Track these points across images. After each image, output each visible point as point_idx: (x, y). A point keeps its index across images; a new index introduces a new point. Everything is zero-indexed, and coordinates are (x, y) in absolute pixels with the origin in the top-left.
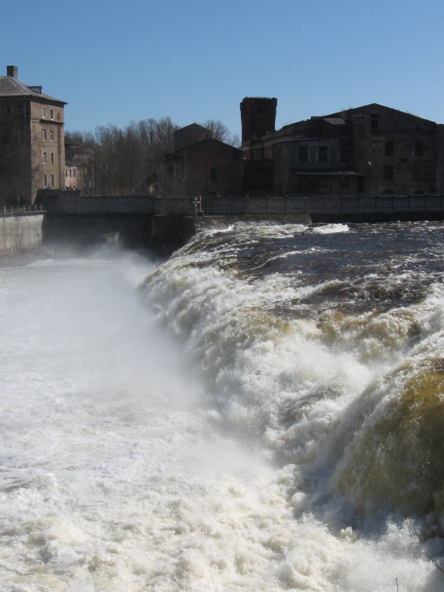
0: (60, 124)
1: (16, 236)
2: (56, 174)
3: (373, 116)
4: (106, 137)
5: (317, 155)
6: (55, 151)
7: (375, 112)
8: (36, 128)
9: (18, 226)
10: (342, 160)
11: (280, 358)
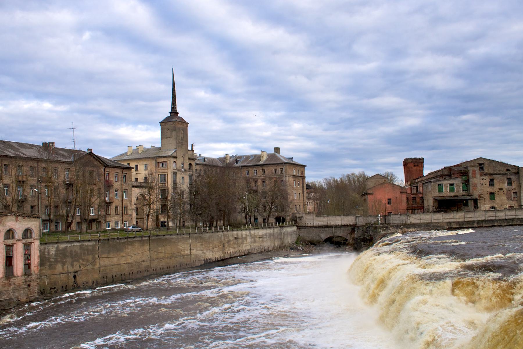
0: (303, 178)
1: (281, 239)
2: (302, 204)
3: (480, 164)
4: (329, 184)
5: (448, 188)
6: (301, 192)
7: (481, 162)
8: (289, 180)
9: (281, 233)
10: (463, 191)
11: (100, 223)
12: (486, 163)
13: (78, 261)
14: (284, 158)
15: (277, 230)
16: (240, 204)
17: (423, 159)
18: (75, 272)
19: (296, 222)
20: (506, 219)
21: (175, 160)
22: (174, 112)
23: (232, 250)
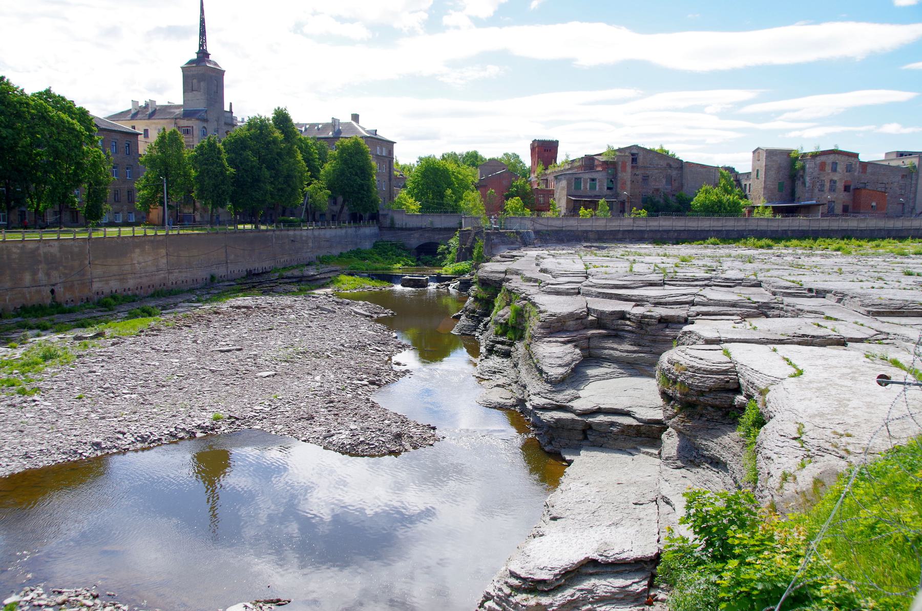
3: (633, 155)
7: (634, 151)
12: (641, 153)
13: (56, 269)
14: (363, 129)
15: (351, 231)
16: (271, 204)
17: (557, 142)
18: (54, 285)
19: (378, 221)
20: (659, 231)
21: (205, 125)
22: (203, 54)
23: (286, 258)
